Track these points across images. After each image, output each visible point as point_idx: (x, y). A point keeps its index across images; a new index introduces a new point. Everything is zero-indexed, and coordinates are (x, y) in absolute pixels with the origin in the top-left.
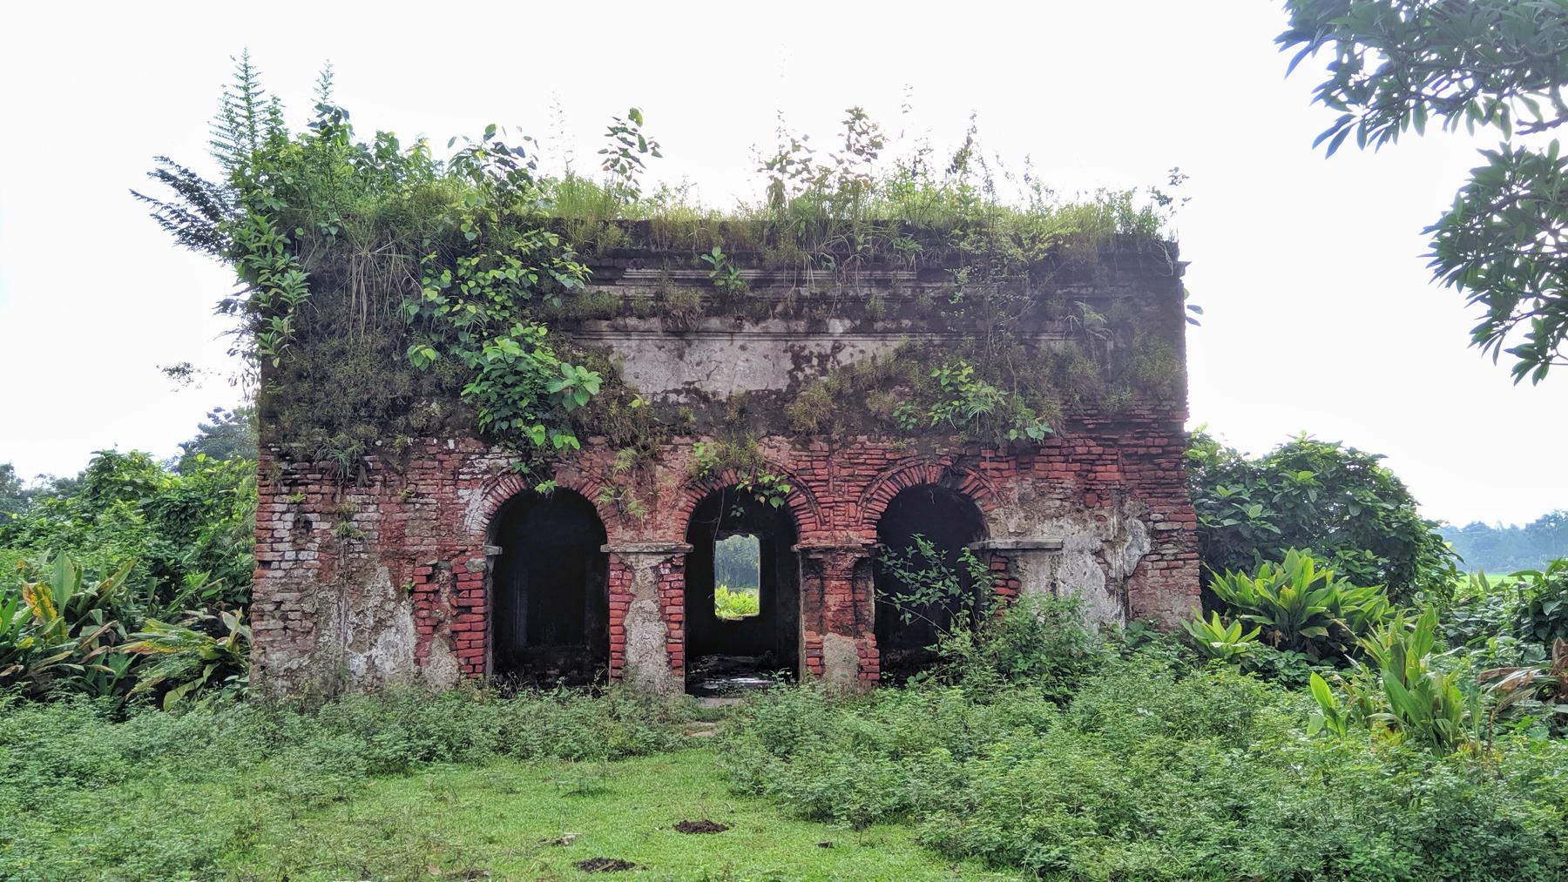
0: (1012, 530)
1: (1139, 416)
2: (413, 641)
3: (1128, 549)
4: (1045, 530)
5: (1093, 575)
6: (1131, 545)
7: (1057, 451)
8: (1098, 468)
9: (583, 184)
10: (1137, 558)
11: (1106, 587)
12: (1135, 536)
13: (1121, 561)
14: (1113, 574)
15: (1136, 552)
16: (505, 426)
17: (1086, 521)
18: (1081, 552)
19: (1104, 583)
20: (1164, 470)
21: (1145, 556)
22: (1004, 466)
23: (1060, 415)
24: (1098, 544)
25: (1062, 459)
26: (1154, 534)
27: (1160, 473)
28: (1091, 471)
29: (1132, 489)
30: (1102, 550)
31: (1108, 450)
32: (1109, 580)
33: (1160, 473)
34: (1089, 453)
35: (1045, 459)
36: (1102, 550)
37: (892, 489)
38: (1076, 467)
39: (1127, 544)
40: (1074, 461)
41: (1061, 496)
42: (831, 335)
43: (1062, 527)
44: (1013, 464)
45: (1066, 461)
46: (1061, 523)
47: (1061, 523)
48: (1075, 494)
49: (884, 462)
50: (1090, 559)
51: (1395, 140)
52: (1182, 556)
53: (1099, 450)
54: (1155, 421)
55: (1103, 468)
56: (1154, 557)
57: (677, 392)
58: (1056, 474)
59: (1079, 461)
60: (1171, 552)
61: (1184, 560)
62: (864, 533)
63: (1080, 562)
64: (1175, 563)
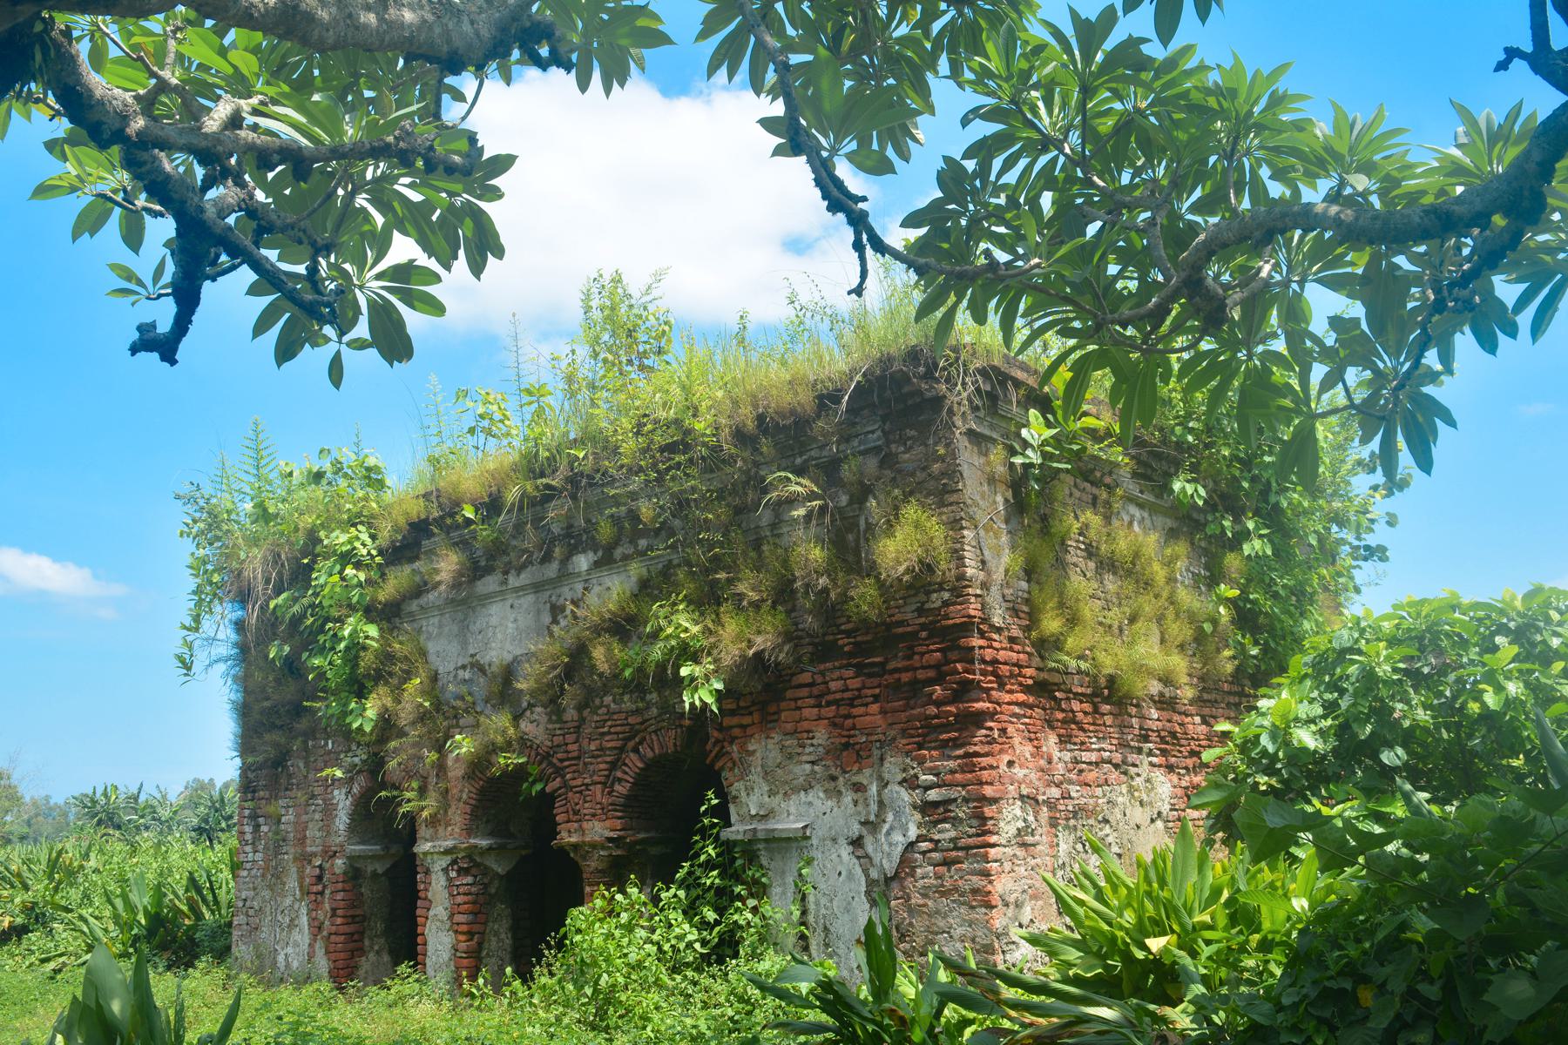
0: (753, 812)
1: (901, 623)
2: (307, 941)
3: (888, 833)
4: (792, 810)
5: (850, 876)
6: (892, 828)
7: (804, 692)
8: (855, 711)
9: (784, 417)
10: (900, 849)
11: (868, 893)
12: (897, 814)
13: (888, 849)
14: (874, 874)
15: (898, 838)
16: (742, 704)
17: (840, 792)
18: (834, 840)
19: (864, 889)
20: (938, 704)
21: (911, 844)
22: (746, 720)
23: (487, 658)
24: (856, 829)
25: (812, 701)
26: (926, 808)
27: (932, 710)
28: (847, 717)
29: (894, 739)
30: (861, 838)
31: (869, 682)
32: (871, 883)
33: (932, 710)
34: (847, 690)
35: (793, 704)
36: (861, 838)
37: (634, 763)
38: (830, 711)
39: (886, 827)
40: (829, 704)
41: (811, 758)
42: (579, 574)
43: (810, 804)
44: (756, 717)
45: (819, 706)
46: (810, 798)
47: (810, 798)
48: (828, 752)
49: (627, 728)
50: (845, 851)
51: (778, 151)
52: (962, 842)
53: (855, 683)
54: (923, 627)
55: (862, 710)
56: (924, 845)
57: (464, 667)
58: (805, 725)
59: (837, 703)
60: (948, 835)
61: (956, 848)
62: (608, 823)
63: (834, 856)
64: (954, 854)
